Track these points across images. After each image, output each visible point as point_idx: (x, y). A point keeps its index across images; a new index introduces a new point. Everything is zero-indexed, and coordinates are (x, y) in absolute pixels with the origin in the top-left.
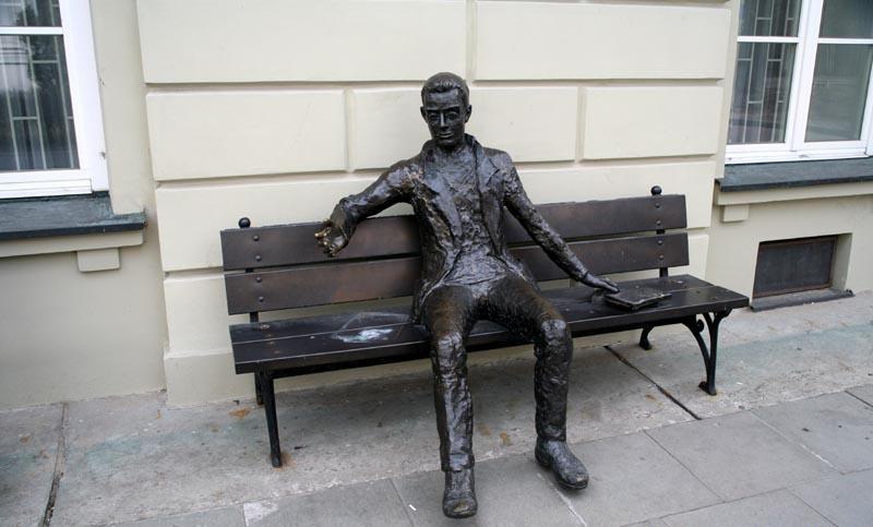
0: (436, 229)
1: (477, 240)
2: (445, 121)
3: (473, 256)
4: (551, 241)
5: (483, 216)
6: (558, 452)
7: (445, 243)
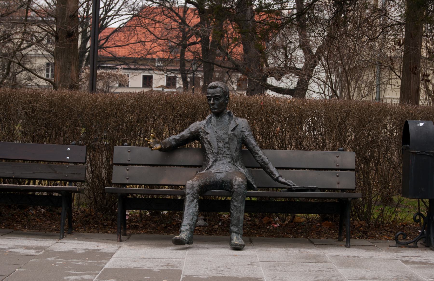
0: (207, 149)
1: (225, 155)
2: (213, 101)
3: (221, 162)
4: (262, 160)
7: (210, 156)
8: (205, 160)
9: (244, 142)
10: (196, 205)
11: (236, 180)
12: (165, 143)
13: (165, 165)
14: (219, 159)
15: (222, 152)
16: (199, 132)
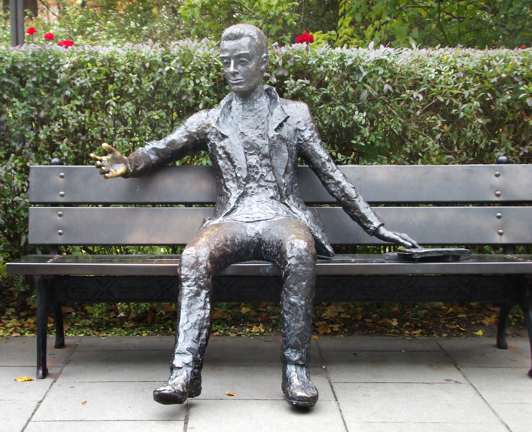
0: (223, 170)
1: (263, 183)
2: (235, 67)
3: (255, 198)
4: (343, 190)
5: (271, 160)
6: (293, 373)
7: (231, 185)
8: (222, 194)
9: (302, 154)
10: (205, 304)
11: (292, 245)
12: (137, 160)
13: (135, 204)
14: (250, 191)
15: (257, 177)
16: (207, 134)
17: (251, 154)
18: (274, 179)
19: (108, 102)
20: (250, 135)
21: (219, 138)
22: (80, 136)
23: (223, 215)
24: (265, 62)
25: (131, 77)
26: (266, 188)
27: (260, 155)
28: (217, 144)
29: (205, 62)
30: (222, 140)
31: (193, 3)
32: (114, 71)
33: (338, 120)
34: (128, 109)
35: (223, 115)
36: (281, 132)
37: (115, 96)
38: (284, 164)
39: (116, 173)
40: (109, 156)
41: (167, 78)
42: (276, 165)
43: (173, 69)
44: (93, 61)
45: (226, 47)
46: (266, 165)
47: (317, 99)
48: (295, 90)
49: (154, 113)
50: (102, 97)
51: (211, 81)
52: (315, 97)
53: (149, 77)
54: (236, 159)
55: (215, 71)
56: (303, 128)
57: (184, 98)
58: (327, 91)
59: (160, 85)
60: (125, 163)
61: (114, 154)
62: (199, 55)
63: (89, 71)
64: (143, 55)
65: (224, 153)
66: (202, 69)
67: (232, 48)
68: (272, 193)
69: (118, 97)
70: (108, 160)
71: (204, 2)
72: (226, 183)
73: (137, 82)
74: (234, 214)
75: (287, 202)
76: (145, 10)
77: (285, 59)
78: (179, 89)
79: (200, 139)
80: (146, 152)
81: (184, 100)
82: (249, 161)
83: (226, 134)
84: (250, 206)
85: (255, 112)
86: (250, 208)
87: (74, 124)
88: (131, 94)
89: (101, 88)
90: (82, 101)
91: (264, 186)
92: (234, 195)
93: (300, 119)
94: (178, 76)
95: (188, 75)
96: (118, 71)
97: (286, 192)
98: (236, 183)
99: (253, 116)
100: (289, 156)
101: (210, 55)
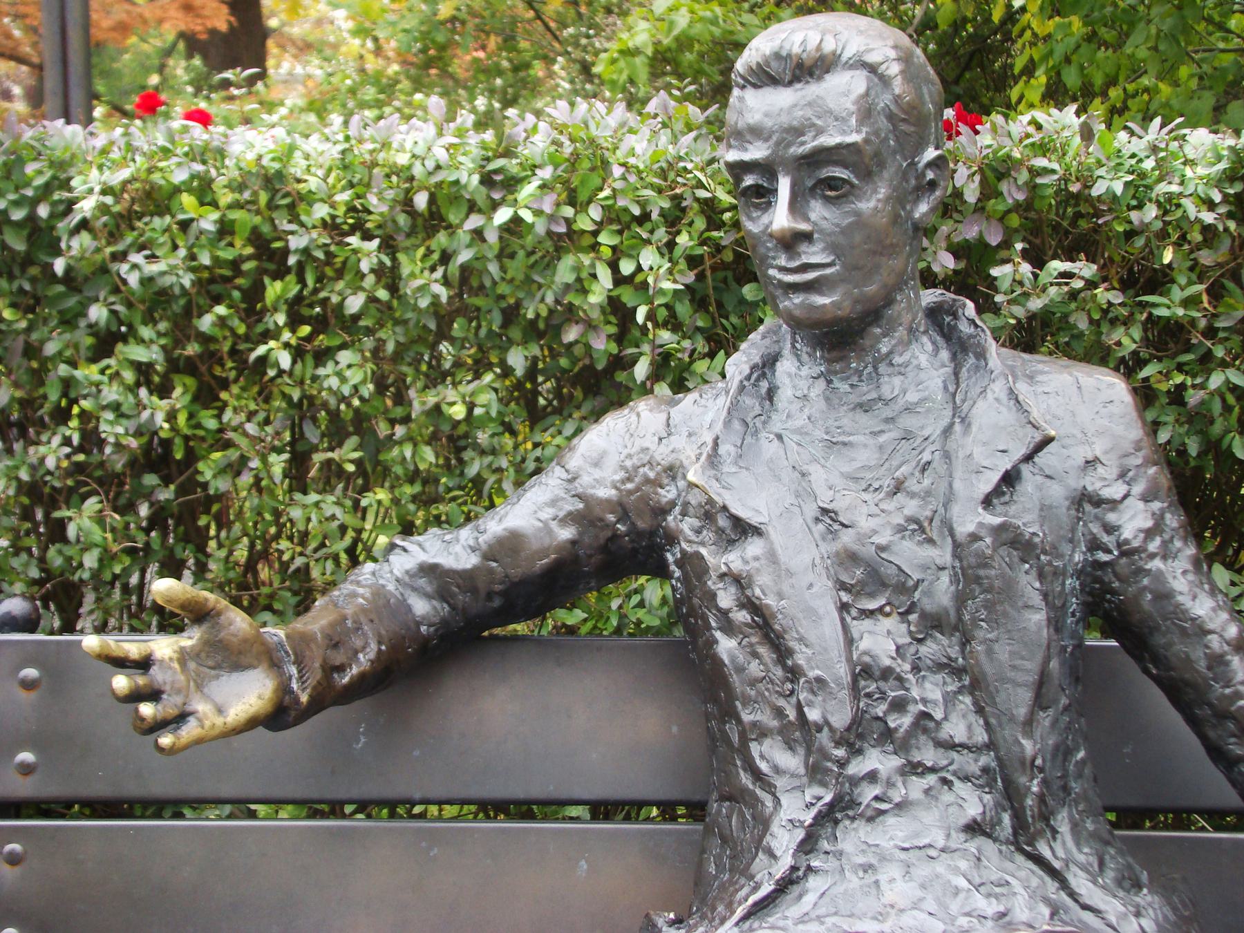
1: (928, 755)
2: (797, 205)
5: (965, 642)
7: (774, 755)
9: (1110, 606)
14: (868, 793)
17: (869, 614)
18: (981, 737)
19: (261, 350)
20: (865, 524)
21: (720, 531)
22: (154, 488)
23: (740, 912)
24: (932, 185)
25: (355, 251)
26: (945, 781)
27: (913, 617)
28: (711, 560)
29: (660, 191)
30: (731, 542)
31: (631, 44)
32: (285, 226)
33: (1217, 428)
34: (343, 380)
35: (737, 425)
36: (1013, 509)
37: (294, 322)
38: (1028, 665)
39: (219, 721)
40: (190, 639)
41: (505, 254)
42: (989, 669)
43: (527, 216)
44: (203, 190)
45: (753, 118)
46: (939, 667)
47: (1126, 341)
48: (1036, 304)
49: (451, 394)
50: (242, 329)
51: (683, 265)
52: (1118, 334)
53: (429, 252)
54: (801, 640)
55: (700, 223)
56: (1116, 491)
57: (571, 334)
58: (1168, 306)
59: (475, 283)
60: (271, 658)
61: (216, 627)
62: (632, 161)
63: (185, 225)
64: (402, 159)
65: (742, 606)
66: (644, 218)
67: (785, 120)
68: (973, 803)
69: (306, 330)
70: (184, 656)
71: (660, 42)
72: (754, 748)
73: (379, 271)
74: (794, 911)
75: (1046, 852)
76: (516, 69)
77: (989, 173)
78: (550, 299)
79: (634, 532)
80: (391, 587)
81: (571, 345)
82: (864, 645)
83: (754, 520)
84: (867, 868)
85: (887, 412)
86: (870, 878)
87: (124, 441)
88: (356, 318)
89: (236, 294)
90: (155, 348)
91: (933, 770)
92: (793, 809)
93: (1098, 448)
94: (549, 245)
95: (587, 241)
96: (302, 225)
97: (1041, 798)
98: (801, 751)
99: (875, 434)
100: (1049, 620)
101: (680, 159)
